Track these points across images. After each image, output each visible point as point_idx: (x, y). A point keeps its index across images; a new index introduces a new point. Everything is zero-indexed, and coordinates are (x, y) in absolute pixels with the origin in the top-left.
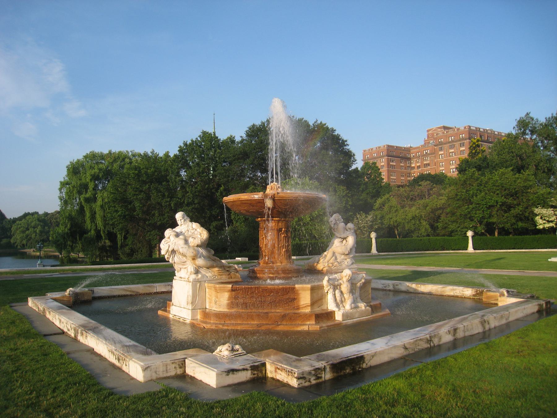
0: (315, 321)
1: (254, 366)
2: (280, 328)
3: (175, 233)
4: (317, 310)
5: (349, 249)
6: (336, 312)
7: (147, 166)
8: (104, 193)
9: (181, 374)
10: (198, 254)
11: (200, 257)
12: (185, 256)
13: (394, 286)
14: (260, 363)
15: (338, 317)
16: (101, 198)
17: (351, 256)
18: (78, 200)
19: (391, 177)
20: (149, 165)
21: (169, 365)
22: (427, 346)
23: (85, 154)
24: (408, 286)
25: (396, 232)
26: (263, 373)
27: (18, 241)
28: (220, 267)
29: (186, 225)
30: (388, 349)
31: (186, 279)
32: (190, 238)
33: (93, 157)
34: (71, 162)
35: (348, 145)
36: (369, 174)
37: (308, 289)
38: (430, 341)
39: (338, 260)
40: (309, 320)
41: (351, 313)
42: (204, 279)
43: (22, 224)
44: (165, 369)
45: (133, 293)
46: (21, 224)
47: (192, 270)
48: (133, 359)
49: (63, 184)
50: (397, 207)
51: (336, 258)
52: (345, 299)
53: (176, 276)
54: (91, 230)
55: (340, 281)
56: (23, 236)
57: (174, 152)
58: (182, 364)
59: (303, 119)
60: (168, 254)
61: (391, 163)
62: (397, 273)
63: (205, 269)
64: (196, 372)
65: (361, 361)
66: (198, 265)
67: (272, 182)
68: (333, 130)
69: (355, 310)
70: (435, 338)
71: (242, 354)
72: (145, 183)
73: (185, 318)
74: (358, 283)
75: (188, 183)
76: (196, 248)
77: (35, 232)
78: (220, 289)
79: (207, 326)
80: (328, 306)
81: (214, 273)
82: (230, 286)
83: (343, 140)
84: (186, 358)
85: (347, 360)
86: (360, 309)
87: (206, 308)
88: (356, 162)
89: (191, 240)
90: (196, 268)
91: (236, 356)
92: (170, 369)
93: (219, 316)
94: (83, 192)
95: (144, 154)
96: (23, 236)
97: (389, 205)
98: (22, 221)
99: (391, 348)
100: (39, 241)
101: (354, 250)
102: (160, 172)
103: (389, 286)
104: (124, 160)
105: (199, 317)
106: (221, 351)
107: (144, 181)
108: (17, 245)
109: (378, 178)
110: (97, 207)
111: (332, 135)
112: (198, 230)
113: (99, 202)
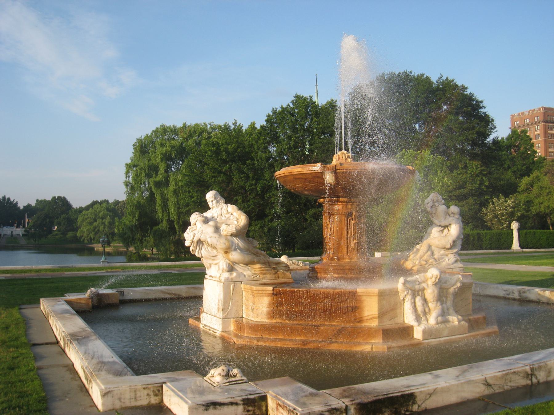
0: (383, 339)
1: (248, 399)
2: (334, 347)
3: (203, 218)
4: (388, 324)
5: (451, 241)
6: (414, 328)
7: (228, 140)
8: (177, 175)
9: (156, 404)
10: (232, 246)
11: (235, 250)
12: (215, 248)
13: (520, 293)
14: (258, 395)
15: (418, 334)
16: (174, 182)
17: (455, 250)
18: (147, 185)
19: (550, 150)
20: (230, 139)
21: (139, 391)
22: (522, 382)
23: (154, 129)
24: (539, 294)
25: (549, 221)
26: (262, 410)
27: (85, 235)
28: (264, 263)
29: (220, 208)
30: (457, 385)
31: (218, 279)
32: (223, 225)
33: (163, 131)
34: (138, 140)
35: (484, 107)
36: (517, 146)
37: (375, 294)
38: (532, 375)
39: (436, 257)
40: (374, 337)
41: (437, 330)
42: (241, 278)
43: (89, 214)
44: (133, 395)
45: (173, 296)
46: (87, 215)
47: (225, 267)
48: (98, 381)
49: (129, 167)
50: (550, 188)
51: (433, 254)
52: (430, 310)
53: (207, 274)
54: (162, 221)
55: (424, 285)
56: (91, 229)
57: (260, 122)
58: (159, 391)
59: (424, 74)
60: (192, 245)
61: (549, 132)
62: (535, 276)
63: (242, 265)
64: (171, 403)
65: (410, 401)
66: (232, 260)
67: (341, 149)
68: (464, 88)
69: (443, 326)
70: (539, 371)
71: (240, 382)
72: (225, 162)
73: (215, 330)
74: (450, 288)
75: (278, 160)
76: (229, 238)
77: (104, 223)
78: (257, 292)
79: (239, 342)
80: (405, 318)
81: (255, 271)
82: (271, 288)
83: (477, 101)
84: (165, 383)
85: (384, 399)
86: (451, 324)
87: (242, 317)
88: (495, 130)
89: (223, 228)
90: (229, 264)
91: (231, 383)
92: (140, 397)
93: (256, 328)
94: (153, 174)
95: (225, 126)
96: (91, 229)
97: (538, 186)
98: (89, 211)
99: (462, 383)
100: (108, 234)
101: (460, 243)
102: (244, 148)
103: (513, 293)
104: (201, 134)
105: (232, 328)
106: (213, 376)
107: (223, 159)
108: (84, 239)
109: (529, 150)
110: (169, 193)
111: (462, 94)
112: (235, 214)
113: (172, 187)
